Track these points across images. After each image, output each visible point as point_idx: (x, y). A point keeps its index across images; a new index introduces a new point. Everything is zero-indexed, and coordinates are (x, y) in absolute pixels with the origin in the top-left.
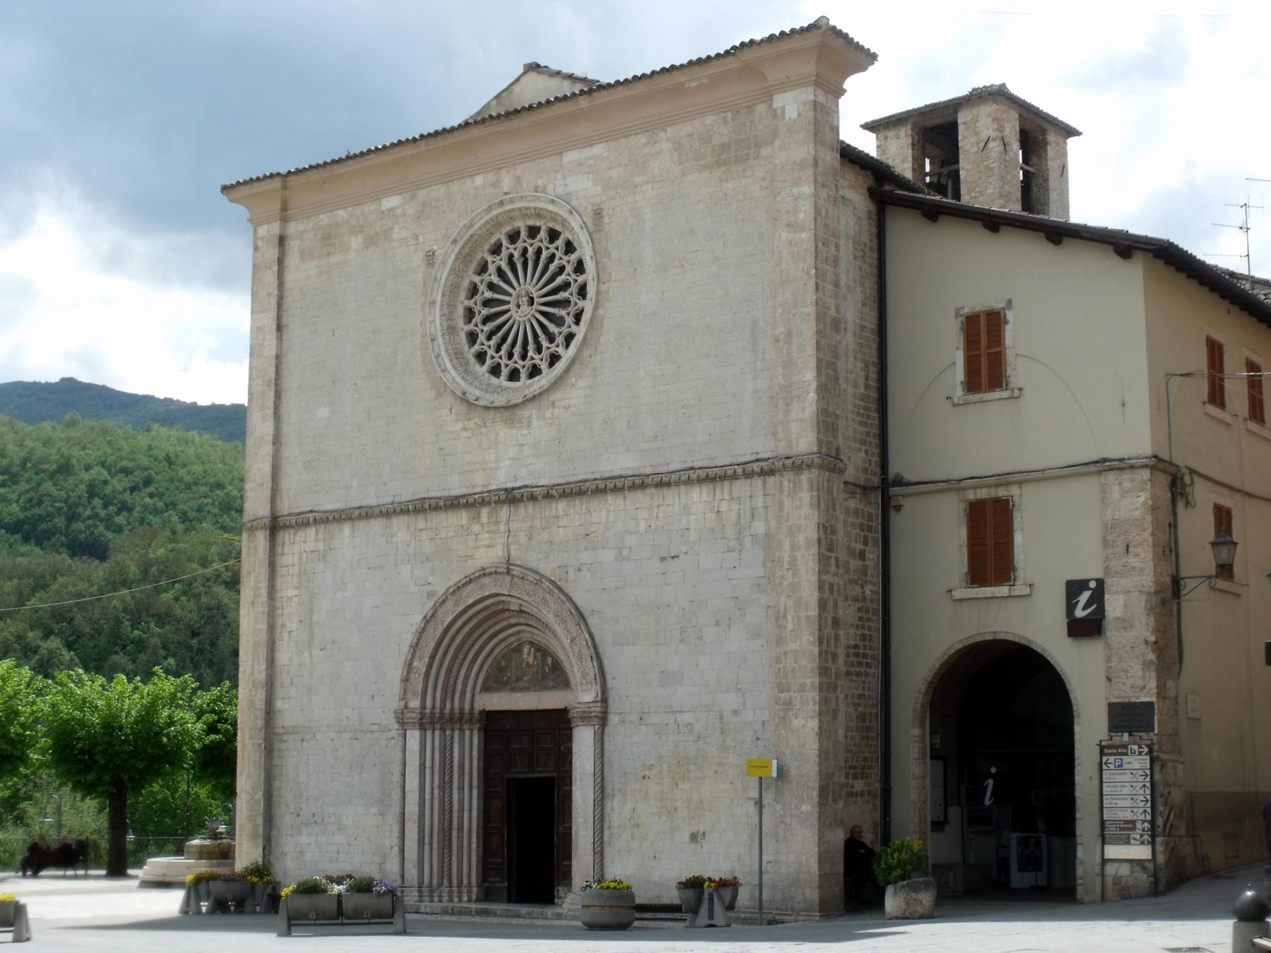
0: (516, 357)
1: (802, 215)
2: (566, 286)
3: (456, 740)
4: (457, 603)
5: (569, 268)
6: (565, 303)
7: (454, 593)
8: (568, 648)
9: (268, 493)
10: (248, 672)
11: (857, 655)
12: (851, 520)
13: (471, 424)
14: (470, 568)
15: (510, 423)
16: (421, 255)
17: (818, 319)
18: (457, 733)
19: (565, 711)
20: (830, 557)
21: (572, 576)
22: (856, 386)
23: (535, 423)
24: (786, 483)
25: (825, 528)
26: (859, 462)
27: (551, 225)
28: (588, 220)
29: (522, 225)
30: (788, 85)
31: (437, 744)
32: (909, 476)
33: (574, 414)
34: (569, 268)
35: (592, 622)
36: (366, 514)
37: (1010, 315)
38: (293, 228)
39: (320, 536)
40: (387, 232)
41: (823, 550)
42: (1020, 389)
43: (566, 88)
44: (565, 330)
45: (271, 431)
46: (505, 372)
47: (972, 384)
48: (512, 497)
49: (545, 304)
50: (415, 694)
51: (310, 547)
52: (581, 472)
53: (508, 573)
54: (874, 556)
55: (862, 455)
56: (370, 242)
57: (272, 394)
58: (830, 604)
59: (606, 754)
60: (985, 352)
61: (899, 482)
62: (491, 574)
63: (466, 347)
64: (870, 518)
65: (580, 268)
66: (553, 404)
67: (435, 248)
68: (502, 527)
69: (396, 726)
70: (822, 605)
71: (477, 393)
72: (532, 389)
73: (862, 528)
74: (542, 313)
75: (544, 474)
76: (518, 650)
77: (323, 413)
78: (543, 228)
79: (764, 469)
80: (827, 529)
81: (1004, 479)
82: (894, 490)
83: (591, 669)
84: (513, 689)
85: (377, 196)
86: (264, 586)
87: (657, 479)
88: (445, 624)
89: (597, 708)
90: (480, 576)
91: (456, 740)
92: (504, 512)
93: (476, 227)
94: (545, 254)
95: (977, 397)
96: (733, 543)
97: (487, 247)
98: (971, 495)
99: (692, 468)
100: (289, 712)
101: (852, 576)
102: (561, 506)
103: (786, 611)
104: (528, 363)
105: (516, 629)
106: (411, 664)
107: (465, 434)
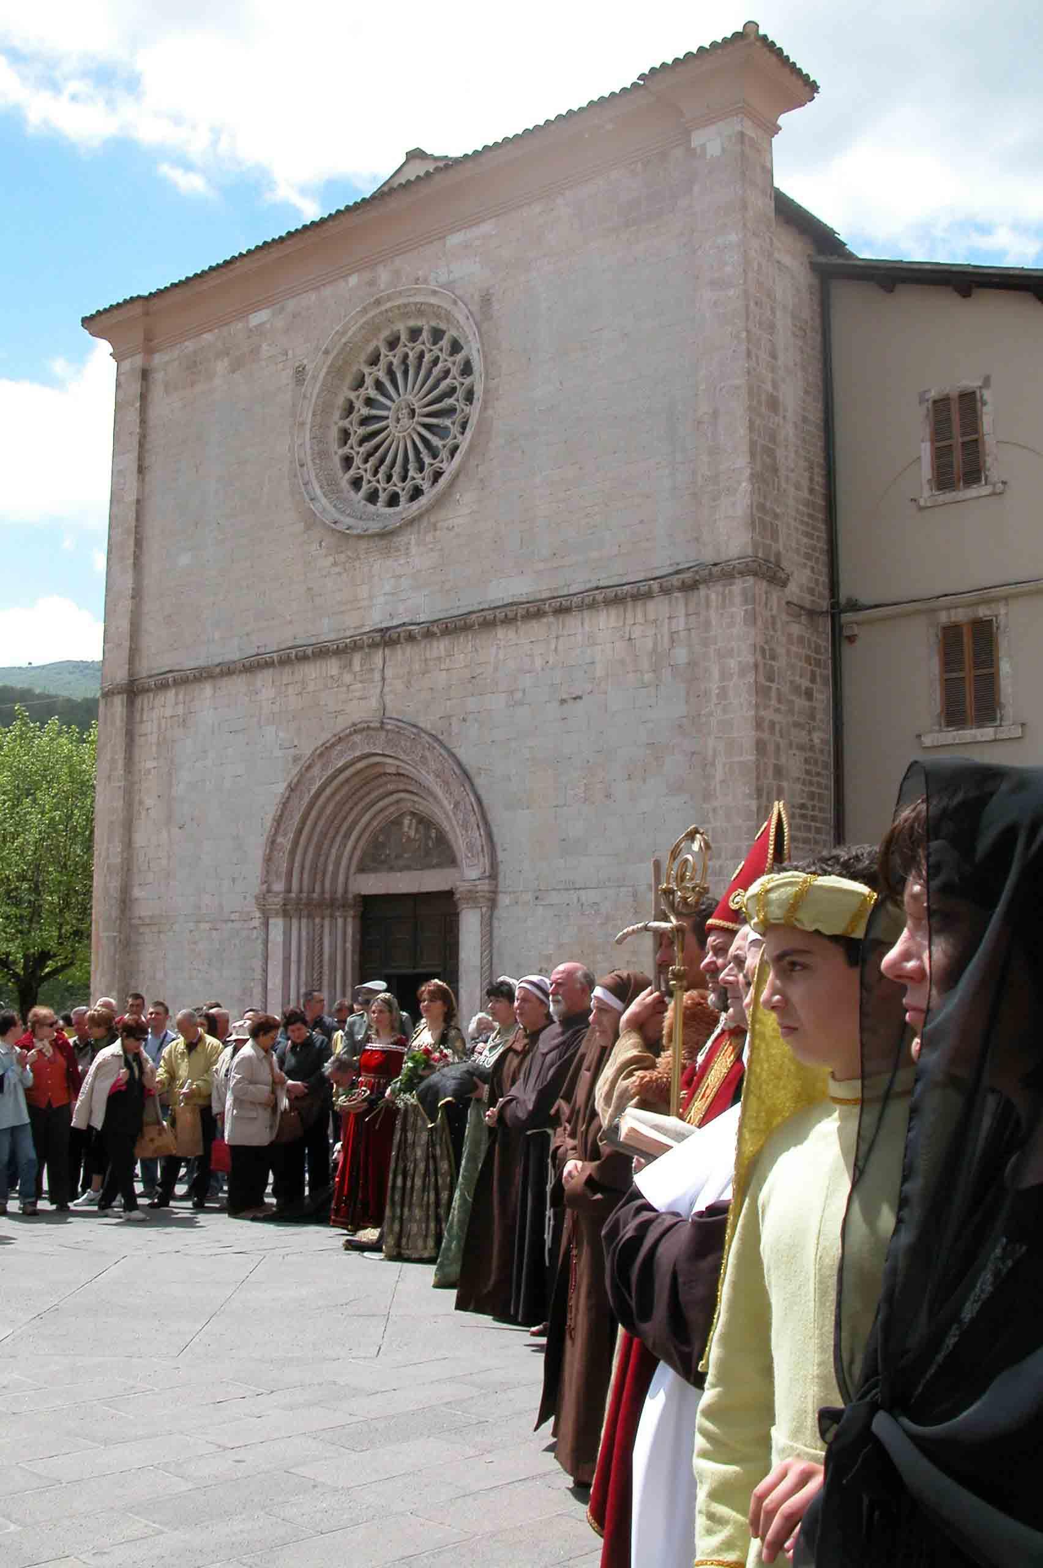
0: (395, 478)
1: (728, 269)
2: (452, 391)
3: (327, 930)
4: (324, 768)
5: (455, 371)
6: (450, 411)
7: (321, 755)
8: (451, 813)
9: (125, 654)
10: (103, 854)
11: (803, 816)
12: (794, 649)
13: (342, 557)
14: (342, 724)
15: (387, 552)
16: (290, 372)
17: (750, 393)
18: (327, 922)
19: (449, 894)
20: (770, 687)
21: (455, 729)
22: (798, 487)
23: (414, 550)
24: (713, 596)
25: (763, 650)
26: (804, 581)
27: (433, 324)
28: (475, 308)
29: (401, 328)
30: (709, 120)
31: (304, 934)
32: (864, 599)
33: (458, 535)
34: (455, 371)
35: (479, 781)
36: (227, 671)
37: (987, 394)
38: (158, 359)
39: (181, 697)
40: (255, 351)
41: (762, 680)
42: (1004, 483)
43: (441, 164)
44: (450, 442)
45: (130, 584)
46: (383, 497)
47: (944, 480)
48: (387, 638)
49: (429, 415)
50: (278, 876)
51: (168, 712)
52: (467, 602)
53: (382, 728)
54: (823, 697)
55: (808, 571)
56: (235, 367)
57: (132, 542)
58: (771, 748)
59: (496, 942)
60: (959, 447)
61: (854, 606)
62: (364, 729)
63: (340, 473)
64: (817, 650)
65: (467, 369)
66: (435, 525)
67: (305, 362)
68: (377, 676)
69: (258, 914)
70: (760, 747)
71: (349, 521)
72: (411, 511)
73: (808, 659)
74: (426, 426)
75: (422, 607)
76: (397, 822)
77: (184, 560)
78: (426, 327)
79: (690, 582)
80: (766, 653)
81: (986, 595)
82: (846, 617)
83: (477, 837)
84: (391, 869)
85: (243, 313)
86: (120, 757)
87: (555, 603)
88: (313, 792)
89: (484, 886)
90: (351, 734)
91: (327, 930)
92: (378, 658)
93: (350, 333)
94: (427, 358)
95: (949, 496)
96: (648, 677)
97: (363, 357)
98: (943, 618)
99: (597, 588)
100: (147, 901)
101: (795, 718)
102: (440, 647)
103: (714, 756)
104: (409, 484)
105: (395, 797)
106: (273, 842)
107: (337, 569)
